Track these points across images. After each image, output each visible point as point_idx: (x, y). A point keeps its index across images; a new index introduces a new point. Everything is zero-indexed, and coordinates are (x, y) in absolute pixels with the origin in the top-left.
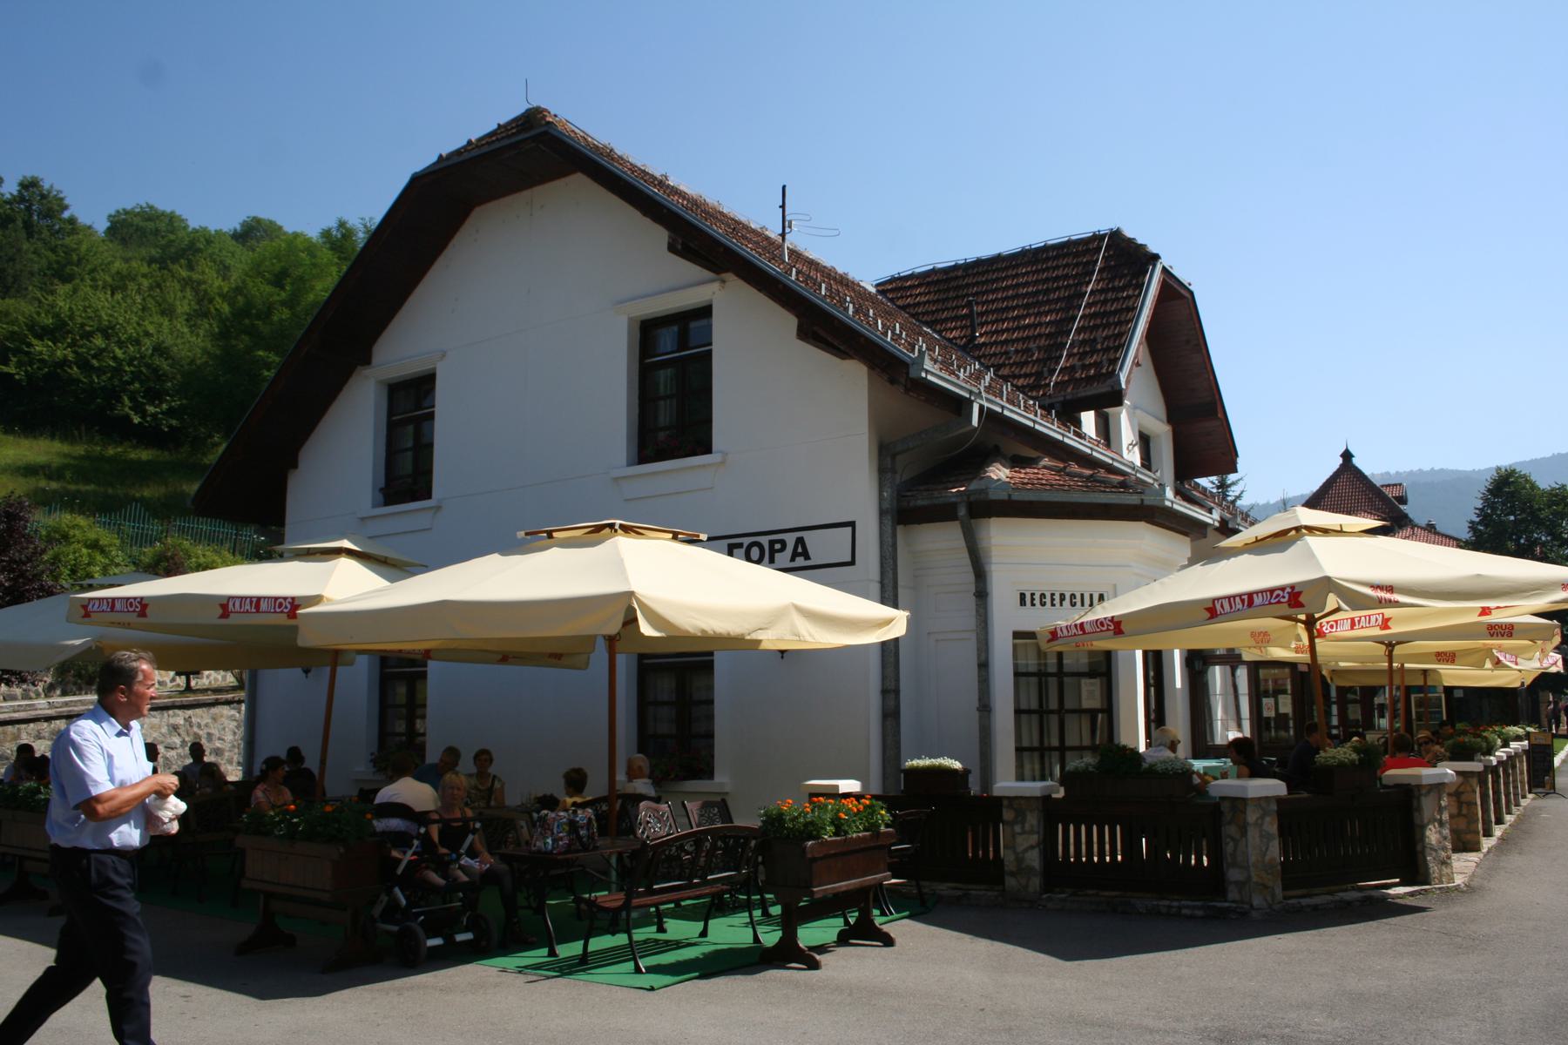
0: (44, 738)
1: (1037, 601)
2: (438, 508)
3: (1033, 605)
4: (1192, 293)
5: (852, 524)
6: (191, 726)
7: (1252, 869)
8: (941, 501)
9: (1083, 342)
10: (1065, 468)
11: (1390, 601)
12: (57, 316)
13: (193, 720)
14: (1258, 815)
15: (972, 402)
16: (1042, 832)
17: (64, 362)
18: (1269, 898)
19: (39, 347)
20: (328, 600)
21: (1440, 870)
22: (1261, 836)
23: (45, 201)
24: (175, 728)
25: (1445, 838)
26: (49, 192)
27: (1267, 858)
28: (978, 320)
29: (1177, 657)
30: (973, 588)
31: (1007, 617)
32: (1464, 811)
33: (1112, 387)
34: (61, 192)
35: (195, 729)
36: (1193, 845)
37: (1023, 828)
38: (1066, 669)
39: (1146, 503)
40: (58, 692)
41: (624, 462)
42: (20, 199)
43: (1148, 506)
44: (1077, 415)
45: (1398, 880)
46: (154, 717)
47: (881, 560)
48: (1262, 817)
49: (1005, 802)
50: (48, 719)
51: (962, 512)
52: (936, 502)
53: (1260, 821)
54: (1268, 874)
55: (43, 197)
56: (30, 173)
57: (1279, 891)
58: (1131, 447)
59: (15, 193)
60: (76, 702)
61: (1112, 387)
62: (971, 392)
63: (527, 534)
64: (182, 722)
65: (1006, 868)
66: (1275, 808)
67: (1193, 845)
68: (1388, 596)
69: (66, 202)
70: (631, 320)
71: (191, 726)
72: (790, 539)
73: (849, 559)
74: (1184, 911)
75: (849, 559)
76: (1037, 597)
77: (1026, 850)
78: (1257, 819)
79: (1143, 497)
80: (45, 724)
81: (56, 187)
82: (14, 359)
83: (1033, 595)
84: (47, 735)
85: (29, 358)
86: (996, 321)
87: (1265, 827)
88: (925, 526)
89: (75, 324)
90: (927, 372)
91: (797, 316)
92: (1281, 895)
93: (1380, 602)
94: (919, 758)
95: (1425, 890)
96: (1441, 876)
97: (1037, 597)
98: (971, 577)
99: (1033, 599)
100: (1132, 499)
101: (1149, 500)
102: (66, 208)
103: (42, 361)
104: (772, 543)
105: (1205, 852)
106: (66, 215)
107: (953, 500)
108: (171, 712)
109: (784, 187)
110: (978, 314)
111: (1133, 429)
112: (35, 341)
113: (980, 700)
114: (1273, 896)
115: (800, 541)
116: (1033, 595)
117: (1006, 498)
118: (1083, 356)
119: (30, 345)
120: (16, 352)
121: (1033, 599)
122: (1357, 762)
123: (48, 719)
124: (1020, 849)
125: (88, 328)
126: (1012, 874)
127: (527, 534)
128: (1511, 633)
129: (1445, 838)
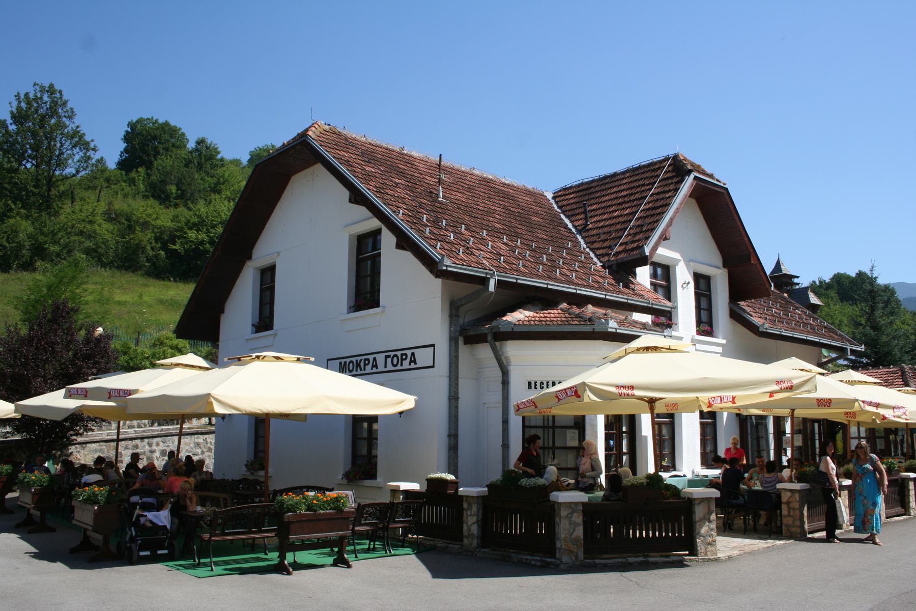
0: (129, 449)
1: (538, 386)
2: (275, 335)
3: (536, 388)
4: (726, 189)
5: (433, 346)
6: (207, 443)
7: (562, 541)
8: (480, 332)
9: (638, 226)
10: (569, 309)
11: (628, 395)
12: (200, 216)
13: (208, 440)
14: (569, 512)
15: (489, 279)
16: (480, 515)
17: (202, 243)
18: (574, 559)
19: (192, 235)
20: (142, 391)
21: (706, 548)
22: (570, 524)
23: (208, 150)
24: (198, 444)
25: (712, 530)
26: (210, 145)
27: (574, 536)
28: (589, 215)
29: (601, 420)
30: (500, 379)
31: (519, 394)
32: (791, 514)
33: (641, 255)
34: (217, 144)
35: (209, 445)
36: (670, 528)
37: (471, 512)
38: (556, 424)
39: (596, 330)
40: (156, 424)
41: (346, 312)
42: (197, 150)
43: (597, 332)
44: (633, 269)
45: (687, 552)
46: (187, 438)
47: (450, 366)
48: (572, 513)
49: (464, 499)
50: (131, 439)
51: (489, 338)
52: (478, 333)
53: (570, 516)
54: (574, 545)
55: (207, 148)
56: (201, 136)
57: (581, 555)
58: (685, 285)
59: (194, 147)
60: (149, 430)
61: (641, 255)
62: (487, 274)
63: (229, 359)
64: (202, 441)
65: (464, 534)
66: (581, 508)
67: (670, 528)
68: (630, 392)
69: (219, 150)
70: (350, 236)
71: (207, 443)
72: (409, 353)
73: (432, 365)
74: (533, 562)
75: (432, 365)
76: (538, 384)
77: (471, 525)
78: (568, 514)
79: (594, 327)
80: (130, 442)
81: (214, 142)
82: (178, 241)
83: (536, 383)
84: (131, 447)
85: (187, 241)
86: (602, 214)
87: (573, 519)
88: (479, 345)
89: (209, 220)
90: (447, 266)
91: (396, 237)
92: (583, 556)
93: (621, 395)
94: (437, 473)
95: (690, 559)
96: (706, 552)
97: (538, 384)
98: (500, 373)
99: (536, 385)
100: (588, 329)
101: (598, 328)
102: (219, 153)
103: (191, 242)
104: (402, 355)
105: (651, 529)
106: (219, 157)
107: (485, 331)
108: (196, 436)
109: (440, 155)
110: (589, 211)
111: (690, 273)
112: (188, 231)
113: (503, 441)
114: (577, 557)
115: (413, 354)
116: (536, 383)
117: (510, 330)
118: (635, 234)
119: (186, 233)
120: (179, 237)
121: (536, 385)
122: (645, 485)
123: (131, 439)
124: (469, 524)
125: (214, 223)
126: (467, 537)
127: (229, 359)
128: (830, 405)
129: (712, 530)
